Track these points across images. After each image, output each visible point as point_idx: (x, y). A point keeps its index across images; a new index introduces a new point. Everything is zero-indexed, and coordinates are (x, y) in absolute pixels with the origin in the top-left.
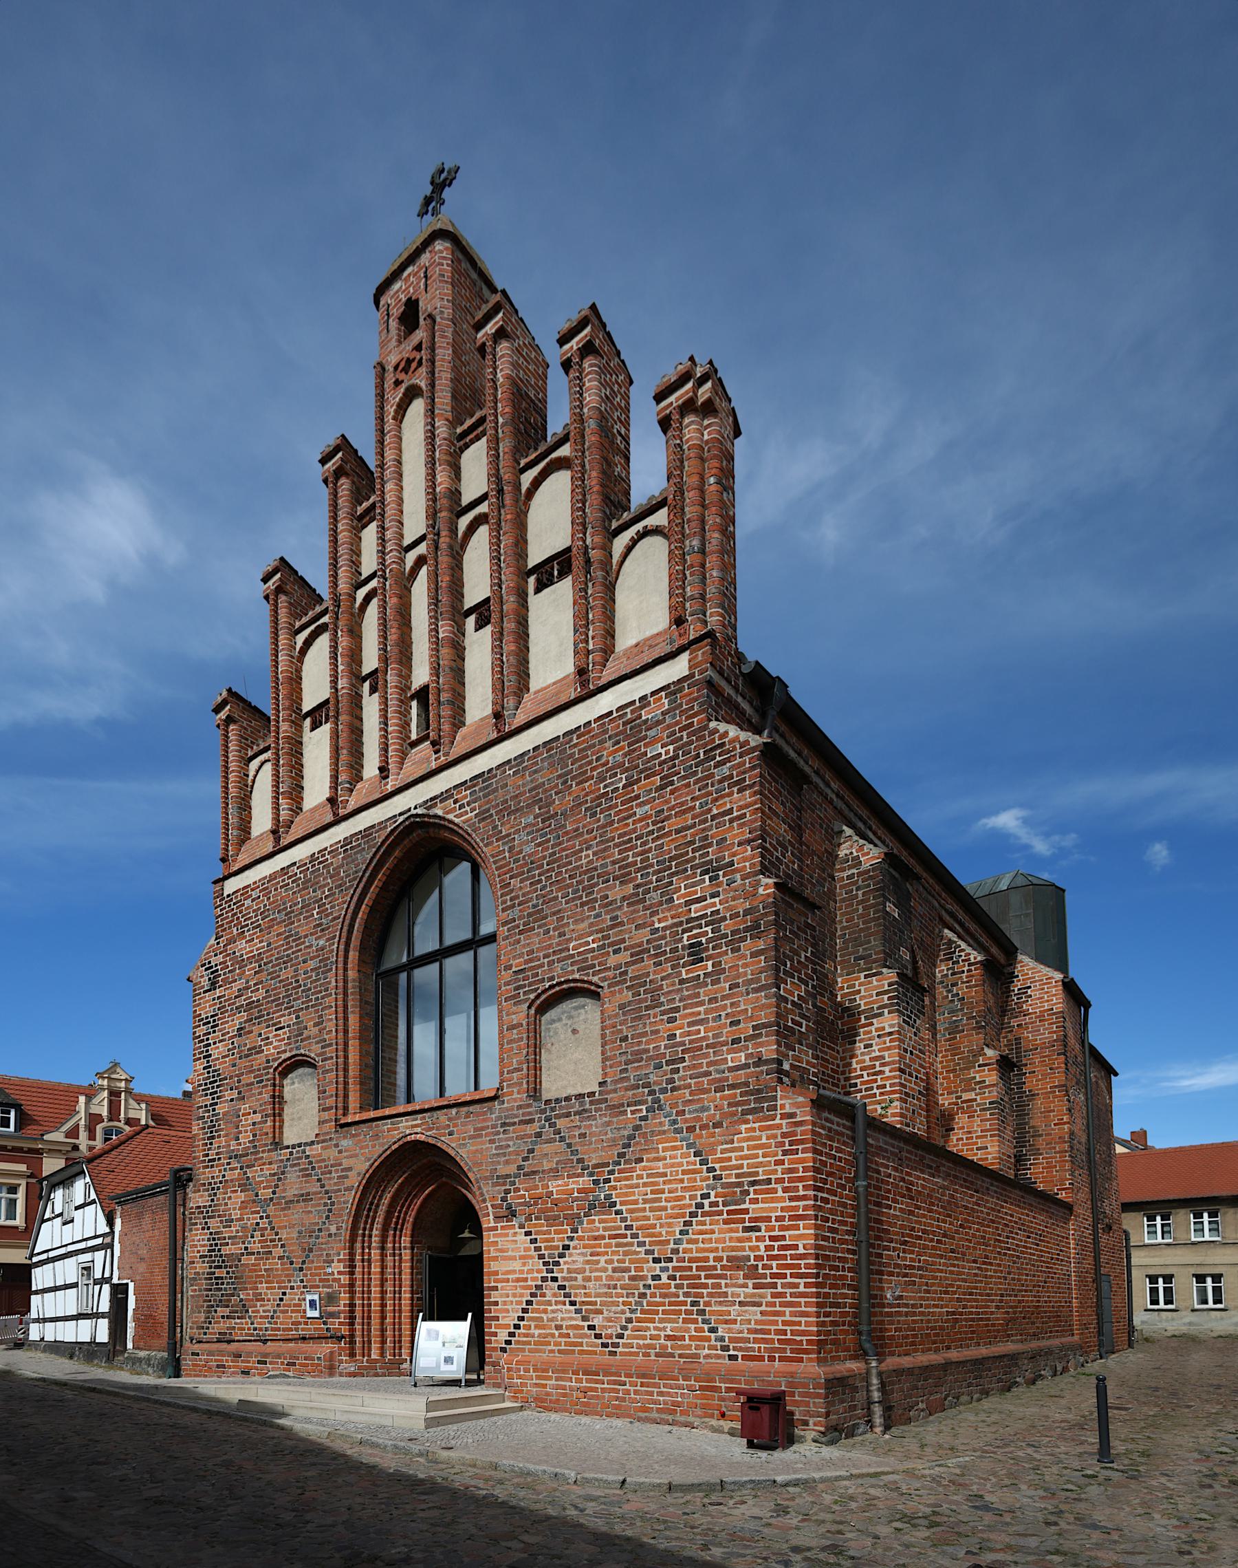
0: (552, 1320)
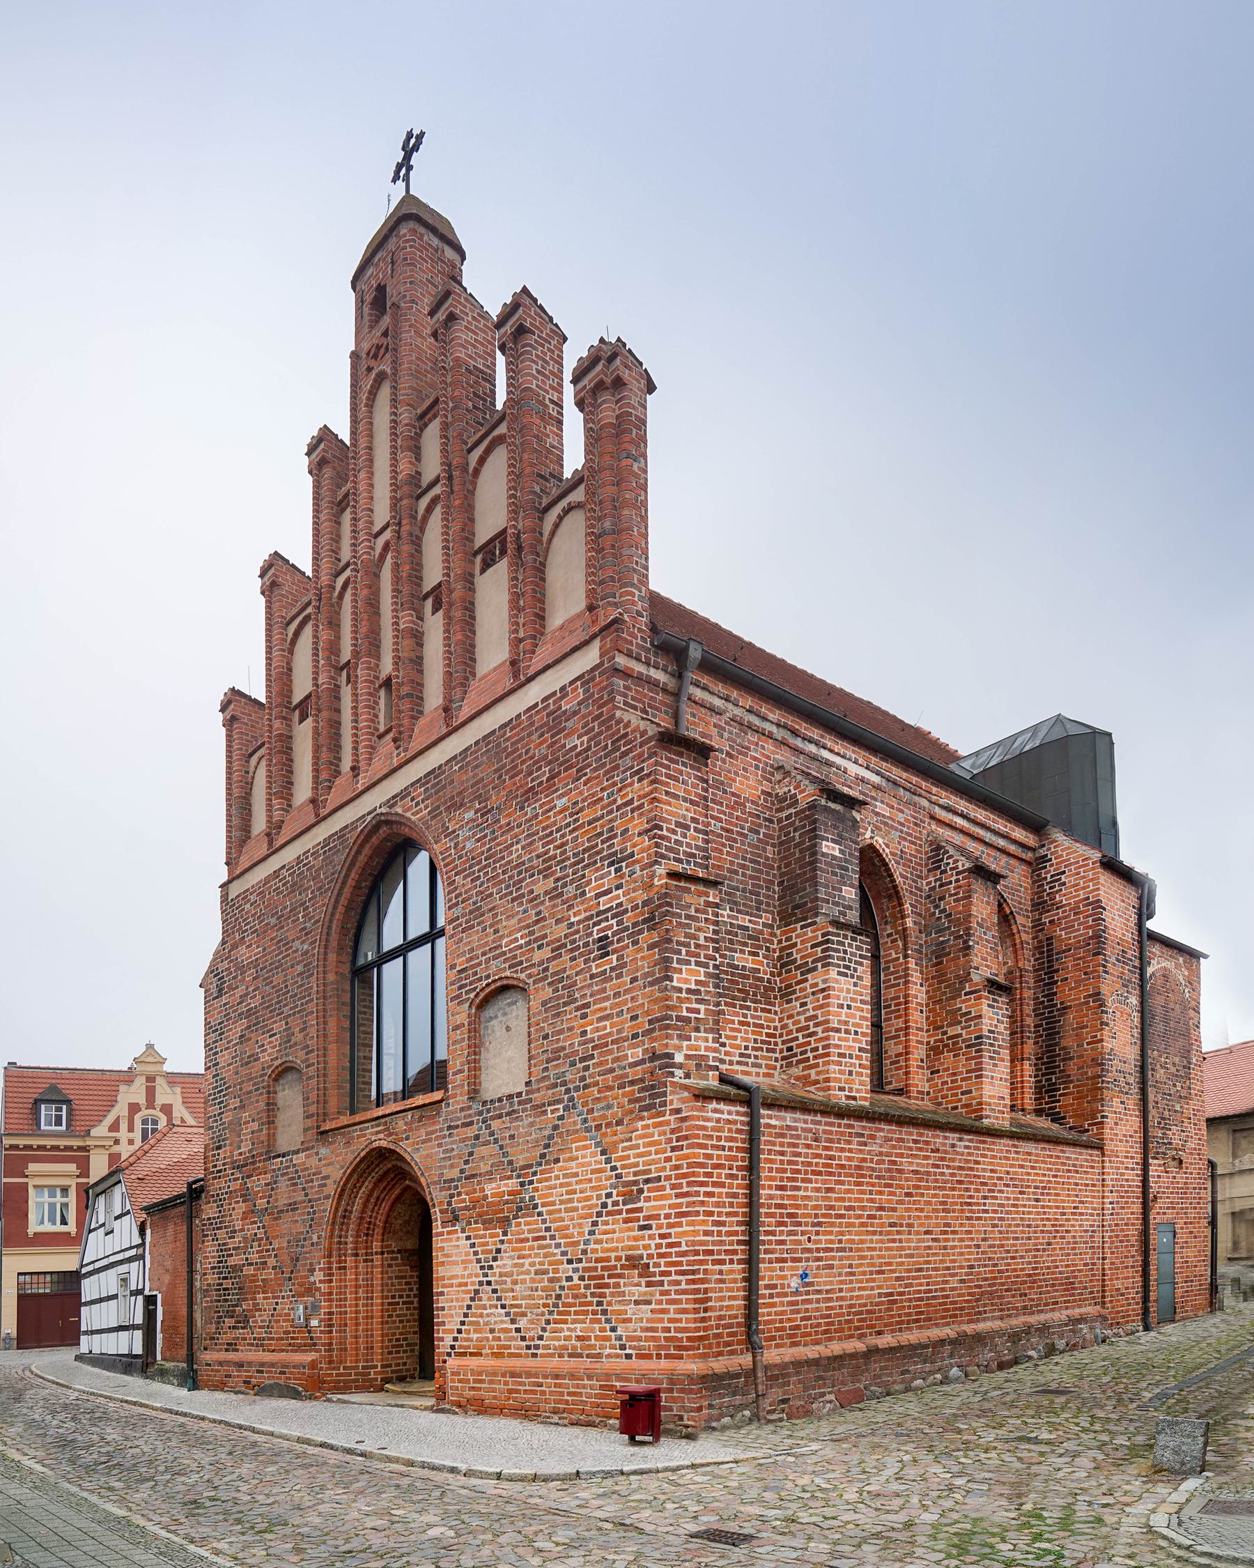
0: (486, 1324)
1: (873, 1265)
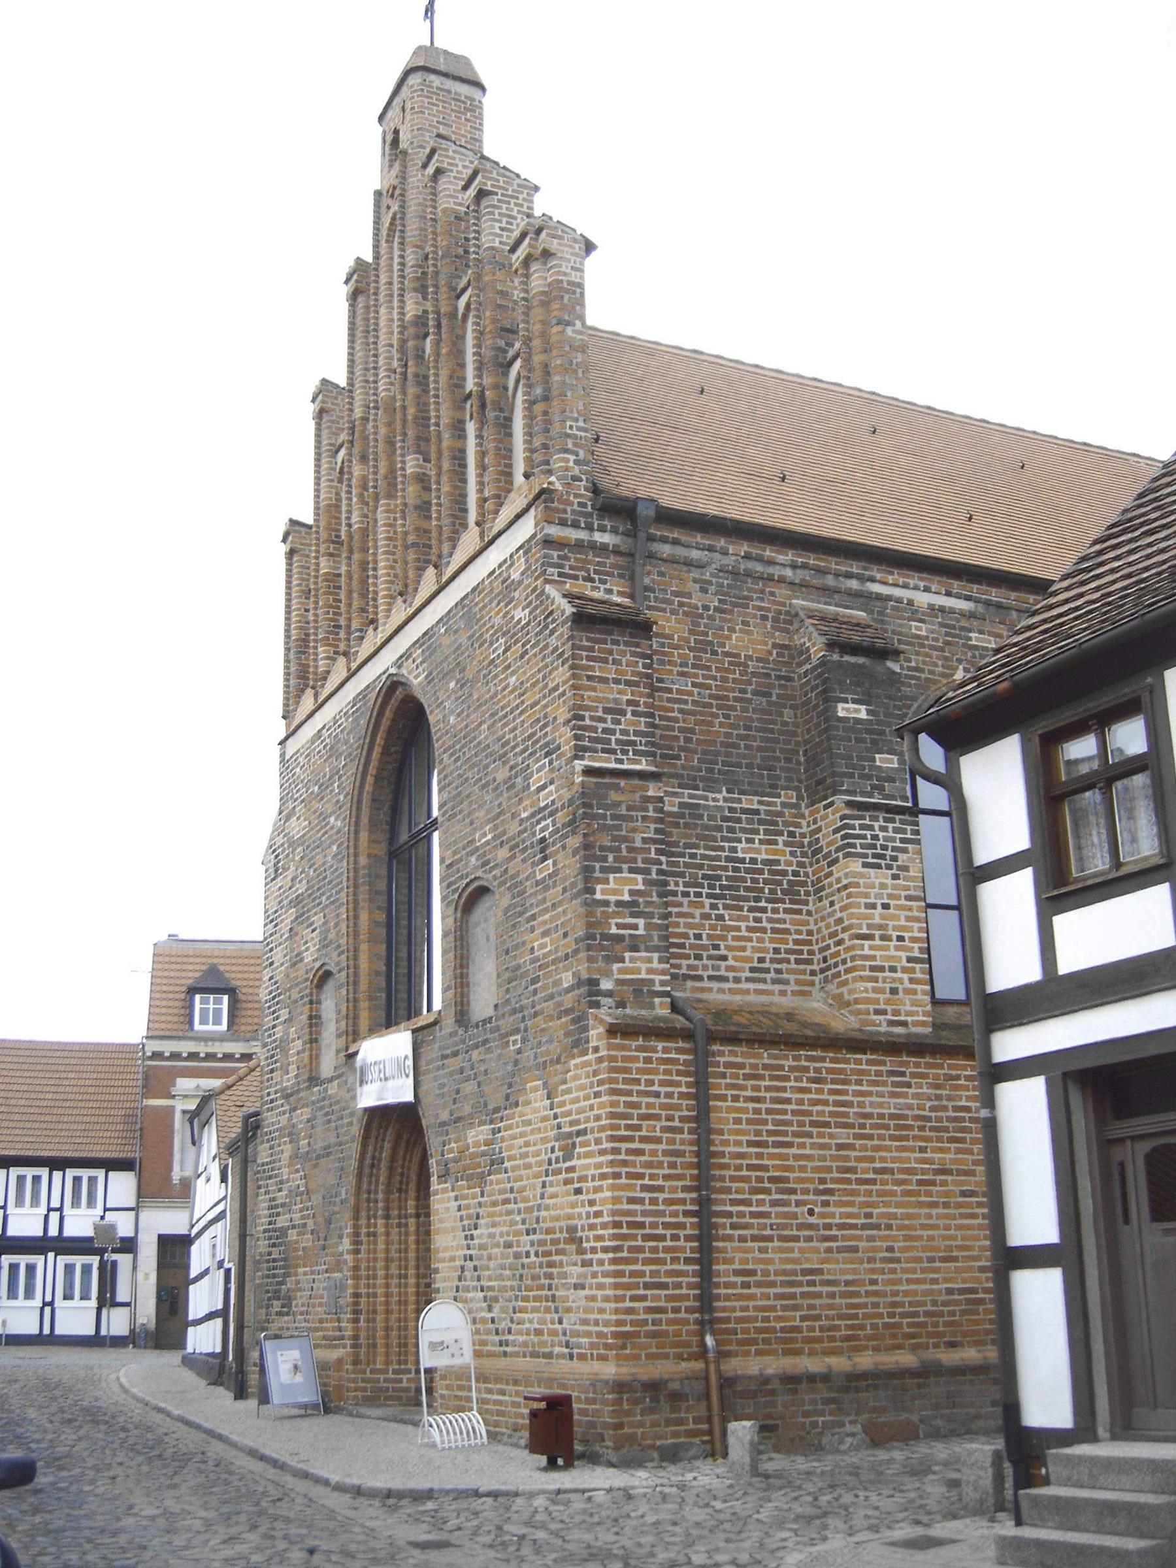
1: (932, 1249)
